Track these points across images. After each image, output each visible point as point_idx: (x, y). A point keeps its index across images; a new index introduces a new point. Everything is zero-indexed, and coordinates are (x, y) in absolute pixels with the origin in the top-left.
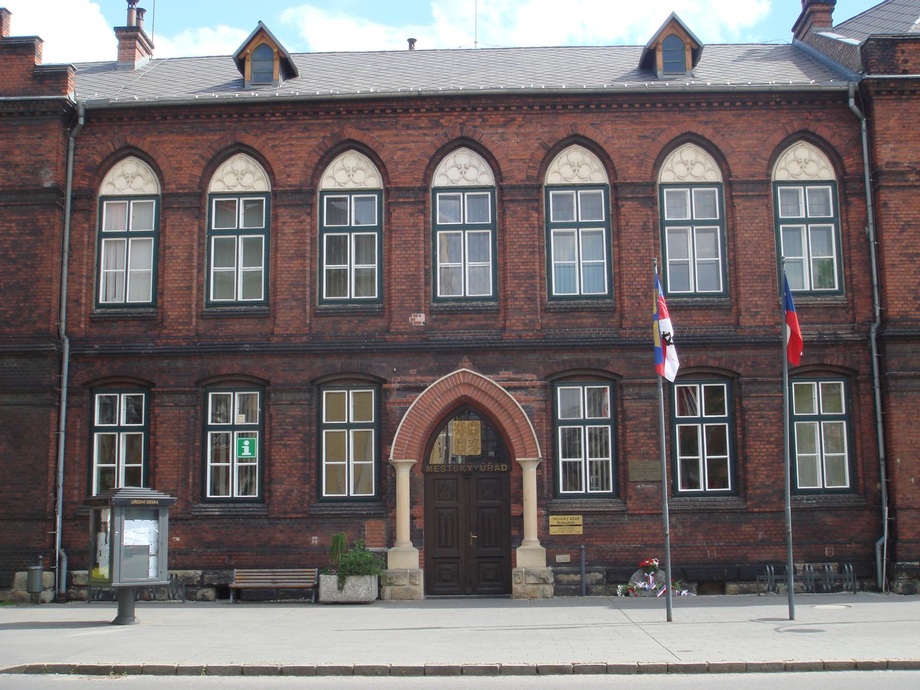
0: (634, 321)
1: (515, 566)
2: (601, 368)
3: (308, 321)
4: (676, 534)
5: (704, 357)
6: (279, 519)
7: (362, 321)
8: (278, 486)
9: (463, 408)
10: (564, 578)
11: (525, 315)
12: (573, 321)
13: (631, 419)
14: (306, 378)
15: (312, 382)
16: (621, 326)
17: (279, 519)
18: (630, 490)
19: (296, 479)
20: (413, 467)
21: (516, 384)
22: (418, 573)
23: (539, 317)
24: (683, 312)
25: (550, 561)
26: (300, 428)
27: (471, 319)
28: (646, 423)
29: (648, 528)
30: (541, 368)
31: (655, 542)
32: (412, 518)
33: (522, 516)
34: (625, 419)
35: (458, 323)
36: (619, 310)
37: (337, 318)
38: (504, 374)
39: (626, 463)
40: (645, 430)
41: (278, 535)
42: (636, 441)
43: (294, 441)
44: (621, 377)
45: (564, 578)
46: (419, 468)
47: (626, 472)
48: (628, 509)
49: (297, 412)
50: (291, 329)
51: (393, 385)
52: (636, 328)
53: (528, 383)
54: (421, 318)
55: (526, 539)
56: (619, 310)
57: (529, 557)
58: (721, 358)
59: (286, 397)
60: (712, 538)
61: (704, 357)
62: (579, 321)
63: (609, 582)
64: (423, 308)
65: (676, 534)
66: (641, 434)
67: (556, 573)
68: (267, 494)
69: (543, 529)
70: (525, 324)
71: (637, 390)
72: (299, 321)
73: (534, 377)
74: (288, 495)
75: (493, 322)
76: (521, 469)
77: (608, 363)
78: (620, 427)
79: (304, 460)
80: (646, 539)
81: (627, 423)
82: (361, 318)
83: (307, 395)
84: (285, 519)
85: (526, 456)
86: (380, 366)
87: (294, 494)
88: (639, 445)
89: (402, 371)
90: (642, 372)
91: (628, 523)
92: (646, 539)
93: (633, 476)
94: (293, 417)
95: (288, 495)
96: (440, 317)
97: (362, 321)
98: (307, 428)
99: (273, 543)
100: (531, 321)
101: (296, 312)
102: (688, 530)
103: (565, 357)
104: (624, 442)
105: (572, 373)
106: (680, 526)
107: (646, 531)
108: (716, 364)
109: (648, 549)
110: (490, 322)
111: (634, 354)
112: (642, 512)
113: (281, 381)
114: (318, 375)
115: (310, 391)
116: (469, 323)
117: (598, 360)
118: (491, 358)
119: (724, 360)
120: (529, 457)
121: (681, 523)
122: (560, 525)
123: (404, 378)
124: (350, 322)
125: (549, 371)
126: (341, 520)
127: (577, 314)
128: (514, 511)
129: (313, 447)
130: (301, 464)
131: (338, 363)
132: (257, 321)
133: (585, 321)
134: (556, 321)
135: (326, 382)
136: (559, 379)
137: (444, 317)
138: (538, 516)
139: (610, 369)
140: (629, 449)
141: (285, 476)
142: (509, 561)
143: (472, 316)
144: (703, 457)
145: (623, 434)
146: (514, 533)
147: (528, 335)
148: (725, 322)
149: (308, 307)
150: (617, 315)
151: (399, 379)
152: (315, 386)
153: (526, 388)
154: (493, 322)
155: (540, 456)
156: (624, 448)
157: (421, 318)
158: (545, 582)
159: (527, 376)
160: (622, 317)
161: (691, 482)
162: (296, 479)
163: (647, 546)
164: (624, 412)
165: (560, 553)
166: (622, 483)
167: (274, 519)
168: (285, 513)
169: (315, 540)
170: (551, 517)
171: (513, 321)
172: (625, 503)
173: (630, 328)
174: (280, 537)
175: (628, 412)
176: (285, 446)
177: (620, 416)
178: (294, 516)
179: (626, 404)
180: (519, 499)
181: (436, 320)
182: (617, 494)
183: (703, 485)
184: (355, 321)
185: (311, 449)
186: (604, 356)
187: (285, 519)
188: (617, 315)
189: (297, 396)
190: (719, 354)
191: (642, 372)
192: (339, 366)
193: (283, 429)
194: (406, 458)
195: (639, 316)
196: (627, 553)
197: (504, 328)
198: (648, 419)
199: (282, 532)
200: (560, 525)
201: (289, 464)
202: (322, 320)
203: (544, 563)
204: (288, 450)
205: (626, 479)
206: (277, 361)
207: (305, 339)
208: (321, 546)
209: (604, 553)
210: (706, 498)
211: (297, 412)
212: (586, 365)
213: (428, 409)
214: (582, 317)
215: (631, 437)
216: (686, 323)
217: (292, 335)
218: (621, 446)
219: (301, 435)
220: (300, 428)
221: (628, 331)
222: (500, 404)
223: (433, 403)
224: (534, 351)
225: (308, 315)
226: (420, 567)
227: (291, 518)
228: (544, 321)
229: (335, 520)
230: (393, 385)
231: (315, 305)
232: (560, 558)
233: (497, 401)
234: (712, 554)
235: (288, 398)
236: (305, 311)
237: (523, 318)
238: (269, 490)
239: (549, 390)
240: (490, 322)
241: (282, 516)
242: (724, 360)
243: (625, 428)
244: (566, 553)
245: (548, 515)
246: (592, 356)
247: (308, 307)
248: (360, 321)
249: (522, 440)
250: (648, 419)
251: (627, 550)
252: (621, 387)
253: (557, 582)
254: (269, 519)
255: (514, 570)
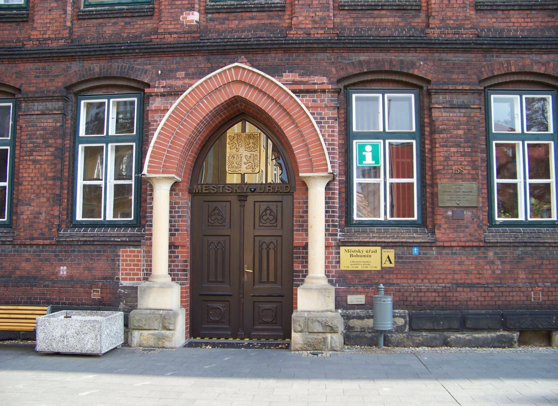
0: (443, 20)
1: (296, 308)
2: (405, 71)
3: (69, 24)
4: (494, 272)
5: (528, 62)
6: (25, 245)
7: (129, 23)
8: (26, 208)
9: (238, 111)
10: (357, 323)
11: (314, 12)
12: (371, 20)
13: (441, 132)
14: (60, 84)
15: (68, 88)
16: (428, 26)
17: (25, 245)
18: (439, 217)
19: (44, 200)
20: (176, 184)
21: (302, 87)
22: (175, 315)
23: (331, 14)
24: (499, 13)
25: (340, 303)
26: (51, 141)
27: (252, 18)
28: (458, 136)
29: (460, 263)
30: (334, 70)
31: (468, 281)
32: (172, 246)
33: (306, 247)
34: (432, 132)
35: (237, 22)
36: (424, 9)
37: (101, 21)
38: (289, 76)
39: (434, 185)
40: (458, 146)
41: (23, 264)
42: (447, 158)
43: (45, 155)
44: (428, 82)
45: (357, 323)
46: (185, 186)
47: (434, 195)
48: (436, 240)
49: (49, 122)
50: (49, 32)
51: (156, 90)
52: (446, 28)
53: (316, 87)
54: (194, 17)
55: (310, 274)
56: (424, 9)
57: (313, 299)
58: (548, 62)
59: (38, 107)
60: (537, 276)
61: (528, 62)
62: (378, 20)
63: (411, 329)
64: (197, 6)
65: (494, 272)
66: (453, 150)
67: (346, 318)
68: (14, 218)
69: (332, 260)
70: (314, 22)
71: (448, 97)
72: (58, 24)
73: (325, 80)
74: (35, 217)
75: (277, 21)
76: (307, 189)
77: (413, 64)
78: (427, 142)
79: (54, 178)
80: (457, 277)
81: (437, 136)
82: (127, 20)
83: (60, 104)
84: (31, 245)
85: (312, 171)
86: (144, 69)
87: (43, 217)
88: (450, 163)
89: (167, 74)
90: (455, 76)
91: (436, 258)
92: (457, 277)
93: (444, 200)
94: (44, 129)
95: (35, 217)
96: (217, 15)
97: (129, 23)
98: (60, 141)
99: (18, 273)
100: (322, 19)
101: (56, 14)
102: (508, 267)
103: (363, 57)
104: (432, 160)
105: (369, 77)
106: (498, 262)
107: (457, 268)
108: (542, 70)
109: (459, 289)
110: (273, 21)
111: (444, 56)
112: (454, 244)
113: (33, 89)
114: (74, 81)
115: (65, 99)
116: (249, 22)
117: (402, 62)
118: (274, 58)
119: (551, 65)
120: (317, 171)
121: (500, 258)
122: (351, 259)
123: (169, 82)
124: (115, 24)
125: (343, 74)
126: (92, 248)
127: (376, 12)
128: (298, 240)
129: (67, 163)
130: (50, 182)
131: (96, 67)
132: (14, 25)
133: (385, 20)
134: (351, 20)
135: (84, 90)
136: (354, 84)
137: (221, 15)
138: (327, 247)
139: (416, 72)
140: (438, 168)
141: (33, 196)
142: (290, 303)
143: (254, 14)
144: (522, 180)
145: (431, 151)
146: (298, 267)
147: (318, 34)
148: (550, 24)
149: (69, 9)
150: (423, 15)
151: (164, 83)
152: (73, 92)
153: (315, 91)
154: (277, 21)
155: (330, 170)
156: (432, 167)
157: (194, 17)
158: (333, 330)
159: (316, 79)
160: (428, 17)
161: (509, 207)
162: (44, 200)
163: (458, 285)
164: (432, 123)
165: (353, 293)
166: (429, 209)
167: (20, 245)
168: (32, 239)
169: (63, 271)
170: (342, 249)
171: (300, 18)
172: (433, 233)
173: (439, 28)
174: (27, 267)
175: (437, 123)
176: (35, 162)
177: (427, 129)
178: (41, 242)
179: (436, 113)
180: (304, 227)
181: (212, 20)
182: (423, 223)
183: (523, 213)
184: (121, 22)
185: (63, 166)
186: (409, 57)
187: (31, 245)
188: (423, 15)
189: (49, 105)
190: (545, 57)
191: (455, 76)
192: (97, 70)
193: (34, 143)
194: (163, 173)
195: (449, 14)
196: (434, 294)
197: (290, 28)
198: (461, 132)
199: (28, 260)
200: (351, 259)
201: (38, 183)
202: (85, 23)
203: (332, 306)
204: (37, 166)
205: (434, 204)
206: (30, 66)
207: (62, 42)
208: (70, 280)
209: (407, 294)
210: (528, 229)
211: (49, 122)
212: (387, 68)
213: (191, 113)
214: (381, 17)
215: (441, 153)
216: (503, 25)
217: (49, 39)
218: (428, 164)
219: (52, 149)
220: (51, 141)
221: (437, 31)
222: (281, 107)
223: (199, 105)
224: (324, 50)
225: (69, 17)
226: (182, 306)
227: (38, 245)
228: (338, 20)
229: (86, 248)
230: (156, 90)
231: (79, 8)
232: (352, 299)
233: (277, 103)
234: (537, 296)
235: (40, 108)
236: (65, 13)
237: (311, 15)
238: (16, 213)
239: (342, 97)
240: (273, 21)
241: (28, 242)
242: (551, 65)
243: (433, 142)
244: (360, 293)
245: (338, 246)
246: (392, 56)
247: (69, 9)
248: (126, 23)
249: (308, 150)
250: (461, 132)
251: (435, 291)
252: (429, 93)
253: (348, 328)
254: (14, 245)
255: (294, 315)
